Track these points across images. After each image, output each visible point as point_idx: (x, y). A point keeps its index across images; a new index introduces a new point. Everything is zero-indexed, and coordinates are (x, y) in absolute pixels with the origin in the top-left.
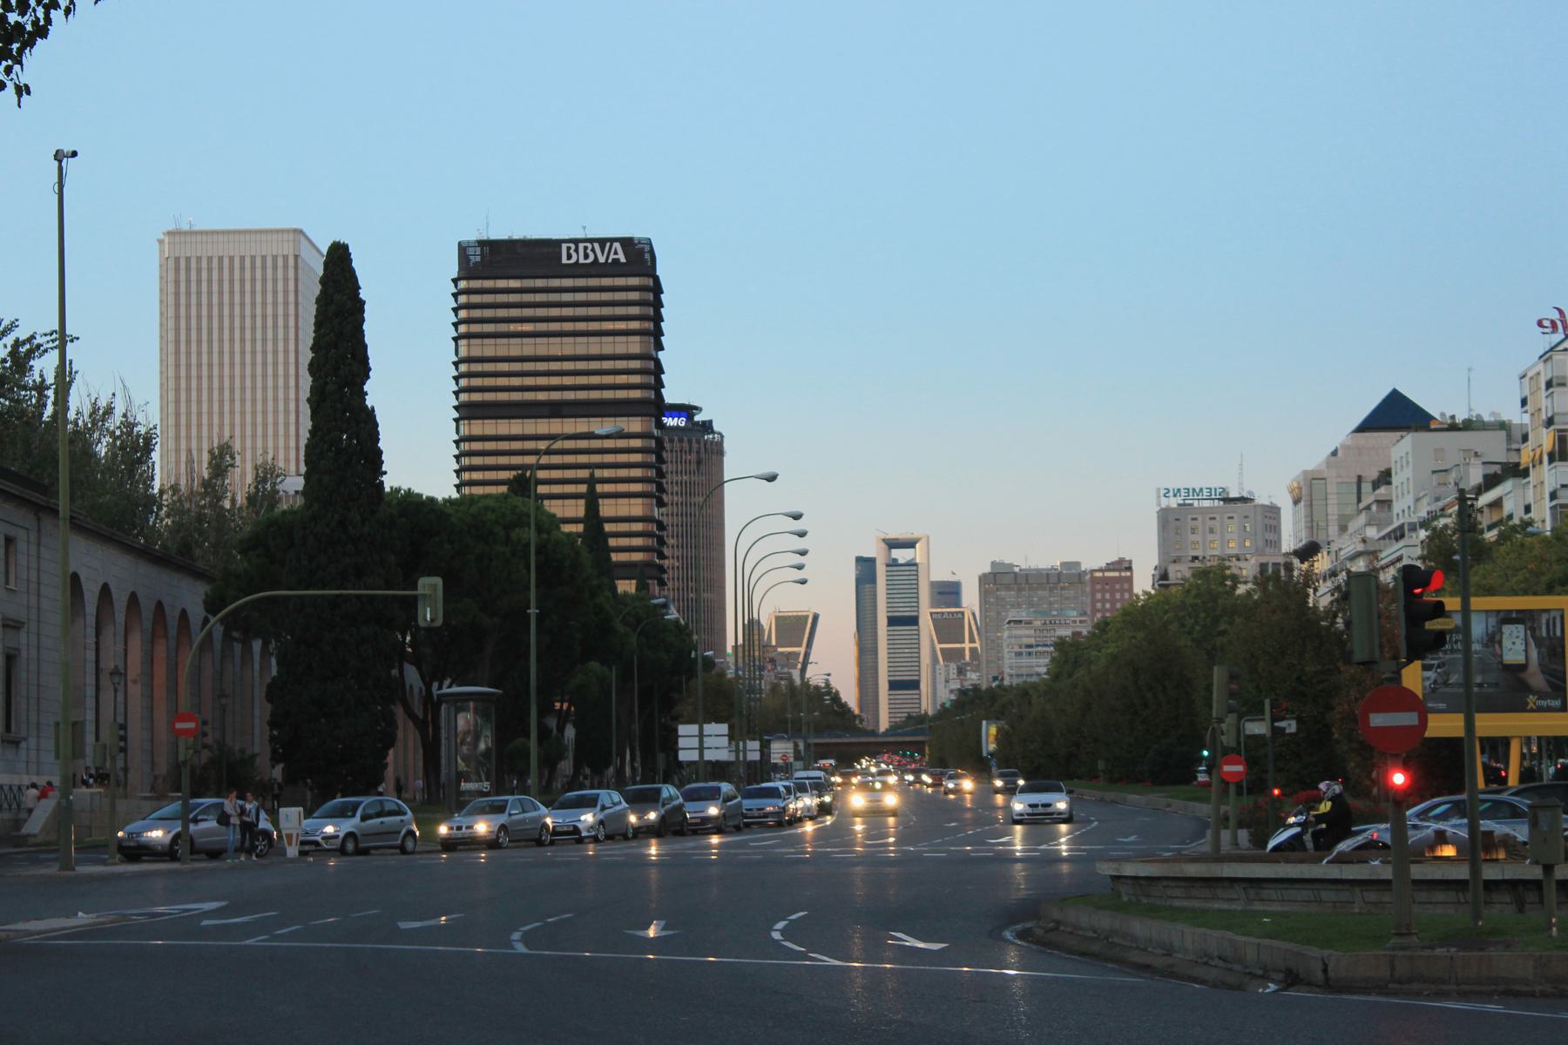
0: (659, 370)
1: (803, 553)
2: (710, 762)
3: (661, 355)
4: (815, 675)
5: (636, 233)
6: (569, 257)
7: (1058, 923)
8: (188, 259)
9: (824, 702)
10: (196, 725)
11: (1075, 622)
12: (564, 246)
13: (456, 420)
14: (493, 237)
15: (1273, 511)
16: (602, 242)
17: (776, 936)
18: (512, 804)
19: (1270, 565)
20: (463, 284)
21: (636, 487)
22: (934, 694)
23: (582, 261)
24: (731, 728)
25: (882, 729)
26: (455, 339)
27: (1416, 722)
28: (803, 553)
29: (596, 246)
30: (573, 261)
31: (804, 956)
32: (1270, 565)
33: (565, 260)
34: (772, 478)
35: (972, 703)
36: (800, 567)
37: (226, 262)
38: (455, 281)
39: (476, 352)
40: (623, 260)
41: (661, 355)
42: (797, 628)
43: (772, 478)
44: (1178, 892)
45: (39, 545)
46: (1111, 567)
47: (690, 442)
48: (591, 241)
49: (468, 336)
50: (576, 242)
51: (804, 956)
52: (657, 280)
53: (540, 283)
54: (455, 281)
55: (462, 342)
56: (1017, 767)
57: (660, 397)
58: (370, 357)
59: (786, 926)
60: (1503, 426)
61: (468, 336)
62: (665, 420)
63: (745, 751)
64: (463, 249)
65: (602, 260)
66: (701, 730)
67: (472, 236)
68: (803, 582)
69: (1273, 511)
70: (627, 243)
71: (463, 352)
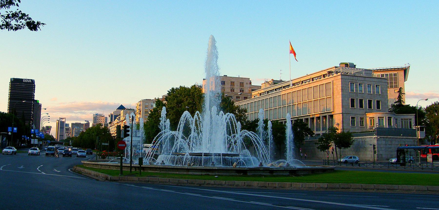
1: (49, 119)
2: (35, 144)
3: (34, 94)
4: (50, 134)
5: (33, 79)
6: (24, 81)
7: (76, 169)
9: (51, 138)
11: (83, 129)
13: (8, 100)
15: (106, 118)
16: (28, 80)
17: (38, 169)
19: (289, 126)
22: (65, 137)
23: (26, 81)
24: (38, 140)
25: (58, 141)
26: (9, 90)
27: (125, 146)
28: (49, 119)
29: (28, 80)
31: (40, 172)
32: (289, 126)
33: (23, 81)
34: (46, 109)
35: (69, 139)
36: (49, 120)
38: (10, 83)
41: (34, 94)
42: (49, 128)
43: (46, 109)
44: (92, 166)
47: (37, 105)
48: (27, 79)
50: (25, 79)
51: (40, 172)
52: (35, 85)
53: (296, 209)
54: (10, 83)
59: (40, 167)
60: (134, 110)
63: (40, 143)
64: (11, 79)
65: (28, 82)
66: (34, 140)
67: (12, 78)
68: (49, 122)
69: (106, 118)
70: (32, 80)
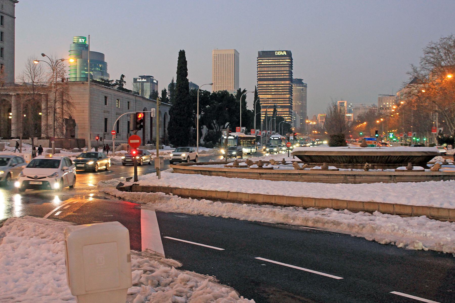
0: (292, 73)
5: (288, 50)
6: (277, 54)
8: (222, 54)
10: (140, 141)
12: (276, 52)
14: (264, 50)
18: (127, 177)
20: (259, 58)
21: (288, 93)
23: (279, 54)
30: (280, 54)
33: (276, 55)
37: (223, 55)
39: (261, 70)
40: (286, 54)
45: (136, 103)
46: (307, 117)
49: (259, 67)
55: (259, 68)
56: (76, 223)
57: (292, 78)
58: (188, 69)
61: (259, 67)
62: (156, 82)
64: (259, 52)
71: (259, 70)
